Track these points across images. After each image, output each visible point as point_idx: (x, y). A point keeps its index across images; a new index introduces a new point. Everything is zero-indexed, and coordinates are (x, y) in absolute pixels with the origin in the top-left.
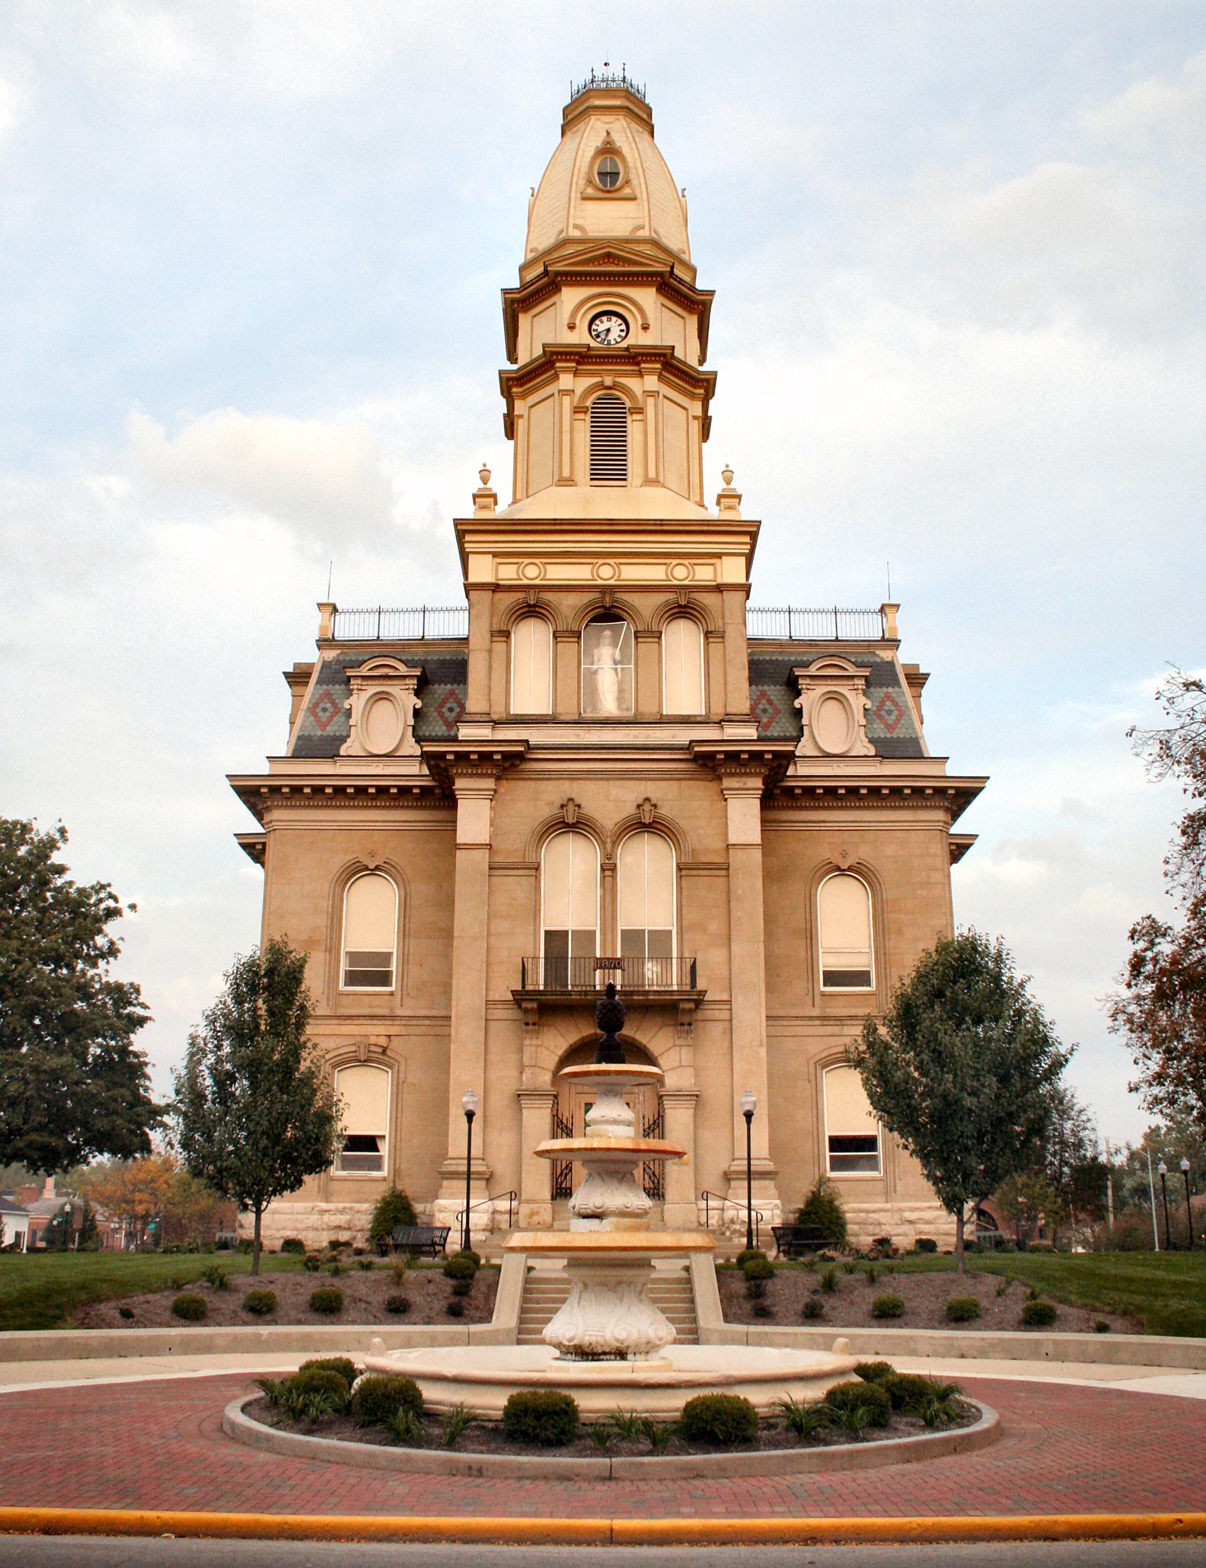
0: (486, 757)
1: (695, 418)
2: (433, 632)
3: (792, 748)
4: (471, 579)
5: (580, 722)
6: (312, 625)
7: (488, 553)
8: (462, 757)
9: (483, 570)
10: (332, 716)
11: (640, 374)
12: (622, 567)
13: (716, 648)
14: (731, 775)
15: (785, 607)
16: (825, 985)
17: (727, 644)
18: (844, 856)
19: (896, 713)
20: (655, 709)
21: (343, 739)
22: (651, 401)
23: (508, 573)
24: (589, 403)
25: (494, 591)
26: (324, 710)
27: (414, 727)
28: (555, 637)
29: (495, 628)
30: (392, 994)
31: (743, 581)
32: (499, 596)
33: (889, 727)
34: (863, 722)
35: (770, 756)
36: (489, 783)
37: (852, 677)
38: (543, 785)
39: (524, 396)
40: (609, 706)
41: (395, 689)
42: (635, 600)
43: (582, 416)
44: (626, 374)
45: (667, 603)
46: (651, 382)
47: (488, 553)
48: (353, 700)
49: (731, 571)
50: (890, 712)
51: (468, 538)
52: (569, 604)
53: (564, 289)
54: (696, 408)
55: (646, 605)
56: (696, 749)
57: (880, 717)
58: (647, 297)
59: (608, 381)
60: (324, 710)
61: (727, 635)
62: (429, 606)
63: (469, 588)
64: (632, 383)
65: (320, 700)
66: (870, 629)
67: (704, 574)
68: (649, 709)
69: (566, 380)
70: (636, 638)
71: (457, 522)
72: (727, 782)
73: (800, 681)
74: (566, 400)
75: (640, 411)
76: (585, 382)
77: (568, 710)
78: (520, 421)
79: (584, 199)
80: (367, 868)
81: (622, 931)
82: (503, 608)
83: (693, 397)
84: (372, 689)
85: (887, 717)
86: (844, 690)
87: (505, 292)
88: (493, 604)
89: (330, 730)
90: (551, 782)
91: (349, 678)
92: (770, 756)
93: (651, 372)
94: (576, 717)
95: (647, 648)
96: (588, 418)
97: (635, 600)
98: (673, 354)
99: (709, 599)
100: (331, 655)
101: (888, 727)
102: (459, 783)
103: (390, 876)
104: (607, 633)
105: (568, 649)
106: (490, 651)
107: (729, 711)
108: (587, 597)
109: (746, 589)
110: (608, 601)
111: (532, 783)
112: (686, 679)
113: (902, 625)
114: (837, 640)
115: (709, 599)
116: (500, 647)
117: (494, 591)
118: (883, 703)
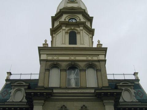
0: (42, 94)
1: (90, 37)
3: (121, 91)
4: (41, 58)
5: (66, 88)
6: (5, 76)
7: (46, 54)
8: (36, 94)
9: (44, 57)
10: (6, 94)
11: (79, 27)
12: (76, 57)
13: (99, 73)
14: (106, 99)
17: (102, 72)
20: (85, 86)
22: (81, 31)
23: (50, 58)
24: (69, 32)
25: (46, 62)
26: (5, 93)
28: (60, 71)
29: (46, 68)
31: (104, 59)
32: (47, 63)
34: (135, 95)
35: (116, 94)
36: (43, 101)
38: (56, 103)
39: (55, 33)
40: (73, 85)
41: (23, 89)
42: (80, 63)
43: (67, 34)
44: (77, 27)
45: (86, 64)
46: (81, 28)
47: (46, 54)
49: (101, 57)
50: (140, 94)
51: (41, 51)
52: (64, 64)
53: (64, 15)
54: (91, 36)
55: (82, 65)
56: (96, 91)
57: (138, 95)
58: (81, 16)
59: (73, 28)
60: (5, 93)
61: (101, 70)
62: (32, 73)
63: (41, 60)
64: (78, 29)
65: (4, 91)
66: (133, 78)
67: (95, 58)
69: (64, 28)
70: (80, 71)
71: (39, 48)
72: (105, 101)
73: (118, 87)
74: (64, 31)
75: (79, 33)
76: (67, 29)
77: (63, 85)
78: (54, 38)
79: (68, 3)
81: (70, 44)
82: (48, 65)
83: (90, 34)
84: (17, 88)
86: (129, 89)
87: (52, 17)
88: (46, 64)
89: (5, 98)
90: (59, 102)
91: (11, 85)
92: (116, 94)
93: (81, 27)
94: (65, 87)
96: (68, 34)
97: (80, 63)
98: (85, 11)
99: (97, 63)
100: (8, 83)
101: (140, 97)
102: (34, 102)
104: (73, 71)
105: (64, 73)
106: (45, 73)
107: (103, 86)
109: (105, 61)
110: (73, 63)
111: (54, 102)
112: (91, 80)
113: (139, 76)
115: (97, 63)
116: (47, 73)
117: (46, 62)
118: (138, 92)
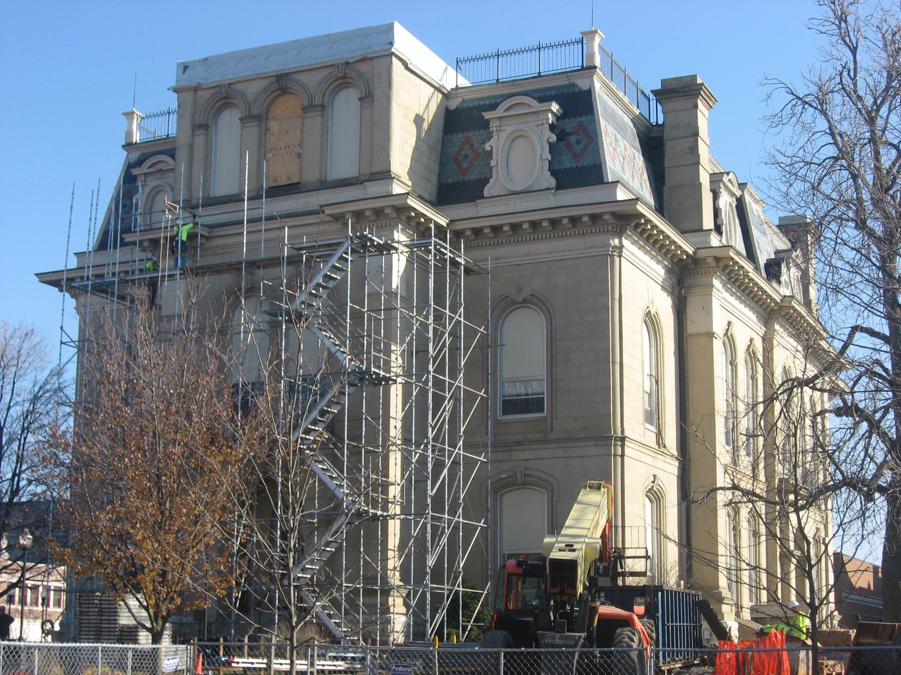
2: (545, 69)
15: (536, 45)
16: (542, 411)
18: (520, 290)
19: (585, 141)
21: (486, 181)
27: (550, 163)
29: (197, 123)
30: (545, 419)
33: (577, 157)
37: (538, 112)
48: (492, 142)
68: (311, 176)
80: (515, 302)
85: (575, 147)
95: (314, 121)
97: (305, 78)
103: (535, 305)
108: (325, 72)
114: (540, 75)
116: (200, 140)
